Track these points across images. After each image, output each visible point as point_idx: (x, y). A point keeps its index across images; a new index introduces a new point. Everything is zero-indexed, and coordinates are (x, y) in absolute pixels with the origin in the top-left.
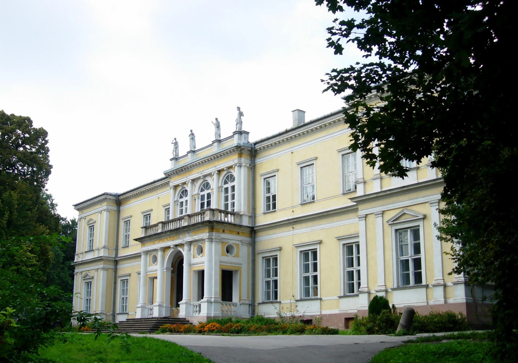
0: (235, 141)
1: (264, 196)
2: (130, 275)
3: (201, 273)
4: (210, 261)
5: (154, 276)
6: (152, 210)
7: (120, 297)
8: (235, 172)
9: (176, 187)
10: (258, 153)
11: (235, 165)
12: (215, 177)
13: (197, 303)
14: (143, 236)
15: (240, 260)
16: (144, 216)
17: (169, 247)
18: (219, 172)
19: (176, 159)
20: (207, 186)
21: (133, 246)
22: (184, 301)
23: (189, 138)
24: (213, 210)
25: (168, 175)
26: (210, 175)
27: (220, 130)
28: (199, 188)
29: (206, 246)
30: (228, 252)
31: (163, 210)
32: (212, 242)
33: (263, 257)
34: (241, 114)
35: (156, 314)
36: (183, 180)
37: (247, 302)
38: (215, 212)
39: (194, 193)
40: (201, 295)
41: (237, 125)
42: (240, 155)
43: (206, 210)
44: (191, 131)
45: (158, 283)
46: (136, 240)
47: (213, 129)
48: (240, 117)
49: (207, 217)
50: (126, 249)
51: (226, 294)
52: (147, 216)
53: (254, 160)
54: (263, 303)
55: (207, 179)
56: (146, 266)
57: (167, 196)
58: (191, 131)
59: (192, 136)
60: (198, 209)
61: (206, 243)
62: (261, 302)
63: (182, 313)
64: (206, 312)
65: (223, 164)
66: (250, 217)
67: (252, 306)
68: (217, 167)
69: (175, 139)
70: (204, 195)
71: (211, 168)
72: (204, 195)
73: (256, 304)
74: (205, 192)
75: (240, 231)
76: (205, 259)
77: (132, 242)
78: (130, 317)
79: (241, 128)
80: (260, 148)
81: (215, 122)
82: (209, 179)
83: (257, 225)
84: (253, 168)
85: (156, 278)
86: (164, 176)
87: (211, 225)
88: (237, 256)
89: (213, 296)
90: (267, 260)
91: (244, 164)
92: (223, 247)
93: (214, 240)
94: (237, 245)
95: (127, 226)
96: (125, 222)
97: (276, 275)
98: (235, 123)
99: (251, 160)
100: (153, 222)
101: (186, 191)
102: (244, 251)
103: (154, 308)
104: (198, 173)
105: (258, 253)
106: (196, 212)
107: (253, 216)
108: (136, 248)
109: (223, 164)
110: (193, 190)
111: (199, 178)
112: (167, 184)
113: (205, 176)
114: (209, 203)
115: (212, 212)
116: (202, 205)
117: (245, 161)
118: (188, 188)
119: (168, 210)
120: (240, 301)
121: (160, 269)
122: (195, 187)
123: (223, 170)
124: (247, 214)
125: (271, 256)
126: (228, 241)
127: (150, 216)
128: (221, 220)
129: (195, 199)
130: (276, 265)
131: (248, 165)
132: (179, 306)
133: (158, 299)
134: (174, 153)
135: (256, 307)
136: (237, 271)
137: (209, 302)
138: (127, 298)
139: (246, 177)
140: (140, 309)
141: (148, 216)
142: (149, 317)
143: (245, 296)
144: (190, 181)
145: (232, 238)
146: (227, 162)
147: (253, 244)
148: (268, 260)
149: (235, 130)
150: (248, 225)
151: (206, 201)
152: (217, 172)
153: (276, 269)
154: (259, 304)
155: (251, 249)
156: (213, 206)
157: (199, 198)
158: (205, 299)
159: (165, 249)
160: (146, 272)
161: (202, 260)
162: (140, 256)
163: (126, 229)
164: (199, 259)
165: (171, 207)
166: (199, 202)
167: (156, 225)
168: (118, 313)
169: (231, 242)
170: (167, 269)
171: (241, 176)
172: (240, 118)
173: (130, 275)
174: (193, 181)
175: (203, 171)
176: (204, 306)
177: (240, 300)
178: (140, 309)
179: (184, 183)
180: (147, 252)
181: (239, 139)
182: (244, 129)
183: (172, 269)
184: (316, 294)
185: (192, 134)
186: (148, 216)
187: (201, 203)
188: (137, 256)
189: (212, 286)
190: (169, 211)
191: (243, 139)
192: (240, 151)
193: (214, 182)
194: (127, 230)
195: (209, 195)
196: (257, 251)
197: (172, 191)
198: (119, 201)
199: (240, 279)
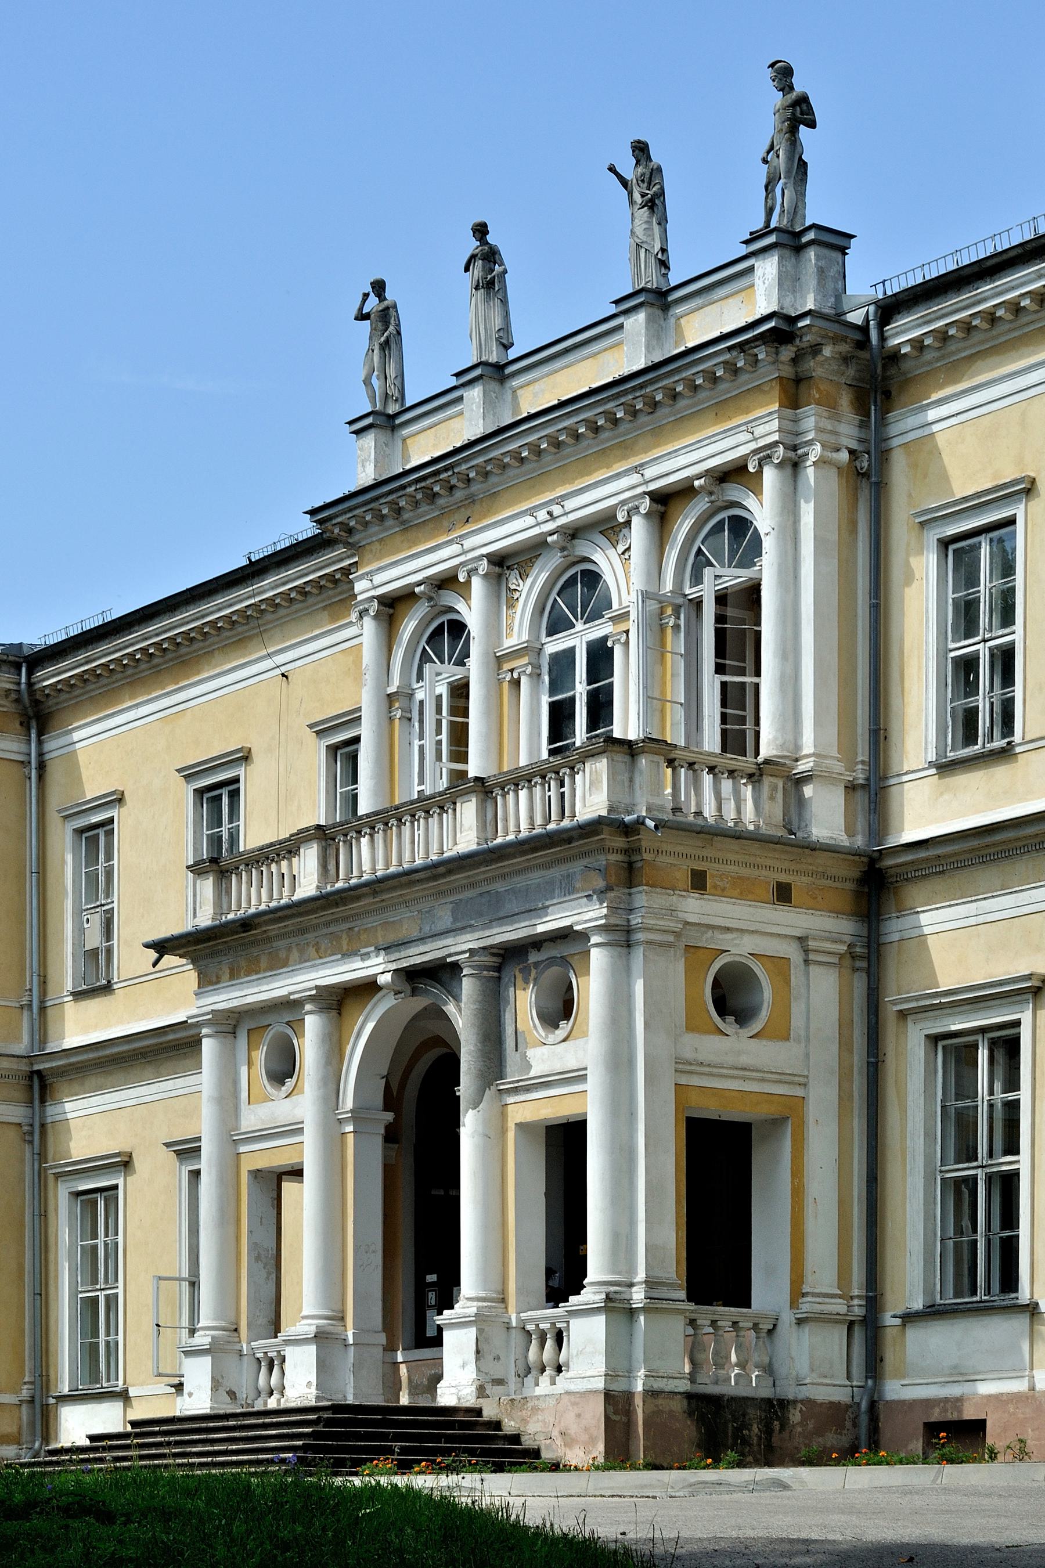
0: (762, 294)
1: (943, 651)
2: (125, 1163)
3: (566, 1142)
4: (619, 1062)
5: (282, 1160)
6: (245, 757)
7: (74, 1293)
8: (763, 511)
9: (392, 606)
10: (907, 382)
11: (764, 454)
12: (639, 532)
13: (548, 1315)
14: (205, 919)
15: (791, 1056)
16: (200, 793)
17: (368, 988)
18: (665, 502)
19: (386, 421)
20: (583, 588)
21: (137, 980)
22: (464, 1307)
23: (467, 280)
24: (629, 748)
25: (343, 525)
26: (608, 526)
27: (663, 222)
28: (539, 608)
29: (594, 983)
30: (722, 1006)
31: (317, 752)
32: (628, 945)
33: (935, 1039)
34: (799, 114)
35: (300, 1384)
36: (586, 500)
37: (839, 1307)
38: (643, 761)
39: (511, 641)
40: (565, 1275)
41: (769, 187)
42: (794, 392)
43: (588, 755)
44: (481, 231)
45: (303, 1201)
46: (162, 947)
47: (619, 215)
48: (793, 131)
49: (591, 795)
50: (94, 1006)
51: (715, 1259)
52: (217, 793)
53: (883, 422)
54: (933, 1312)
55: (583, 548)
56: (229, 1102)
57: (339, 662)
58: (481, 231)
59: (487, 265)
60: (532, 744)
61: (595, 954)
62: (918, 1305)
63: (457, 1385)
64: (599, 1366)
65: (688, 455)
66: (851, 788)
67: (869, 1330)
68: (649, 473)
69: (379, 287)
70: (572, 650)
71: (611, 487)
72: (572, 650)
73: (889, 1320)
74: (578, 639)
75: (799, 883)
76: (587, 1061)
77: (131, 958)
78: (140, 1412)
79: (797, 209)
80: (918, 344)
81: (628, 168)
82: (605, 560)
83: (892, 842)
84: (867, 476)
85: (297, 1173)
86: (306, 529)
87: (619, 853)
88: (779, 1031)
89: (641, 1276)
90: (957, 1052)
91: (815, 452)
92: (692, 973)
93: (640, 936)
94: (779, 965)
95: (92, 857)
96: (80, 832)
97: (1012, 1147)
98: (762, 173)
99: (864, 425)
100: (256, 831)
101: (458, 628)
102: (821, 997)
103: (289, 1352)
104: (531, 512)
105: (903, 1015)
106: (523, 762)
107: (872, 791)
108: (167, 998)
109: (688, 455)
110: (500, 624)
111: (536, 548)
112: (340, 583)
113: (574, 533)
114: (600, 708)
115: (621, 758)
116: (560, 716)
117: (827, 431)
118: (473, 611)
119: (345, 755)
120: (794, 1304)
121: (311, 1116)
122: (511, 604)
123: (684, 492)
124: (838, 767)
125: (983, 1030)
126: (722, 941)
127: (234, 795)
128: (738, 821)
129: (516, 683)
130: (1012, 1083)
131: (844, 456)
132: (437, 1342)
133: (305, 1303)
134: (376, 383)
135: (890, 1335)
136: (776, 1123)
137: (616, 1306)
138: (112, 1301)
139: (1013, 354)
140: (206, 1361)
141: (225, 793)
142: (259, 1406)
143: (822, 1272)
144: (484, 566)
145: (749, 927)
146: (712, 439)
147: (870, 957)
148: (957, 1052)
149: (759, 224)
150: (844, 840)
151: (581, 689)
152: (646, 504)
153: (1013, 1108)
154: (909, 1318)
155: (860, 984)
156: (628, 722)
157: (536, 676)
158: (589, 1295)
159: (342, 1000)
160: (233, 1141)
161: (571, 1063)
162: (195, 1044)
163: (92, 879)
164: (543, 1054)
165: (367, 731)
166: (534, 707)
167: (289, 848)
168: (66, 1390)
169: (740, 949)
170: (358, 1115)
171: (794, 537)
172: (794, 142)
173: (125, 1163)
174: (504, 564)
175: (559, 500)
176: (588, 1336)
177: (797, 1294)
178: (206, 1361)
179: (447, 582)
180: (232, 1023)
181: (788, 282)
182: (820, 209)
183: (389, 1116)
184: (1010, 1281)
185: (490, 256)
186: (225, 793)
187: (554, 707)
188: (166, 1049)
189: (631, 1219)
190: (353, 760)
191: (810, 280)
192: (794, 361)
193: (625, 573)
194: (98, 884)
195: (600, 657)
196: (893, 999)
197: (367, 632)
198: (36, 703)
199: (797, 1172)
